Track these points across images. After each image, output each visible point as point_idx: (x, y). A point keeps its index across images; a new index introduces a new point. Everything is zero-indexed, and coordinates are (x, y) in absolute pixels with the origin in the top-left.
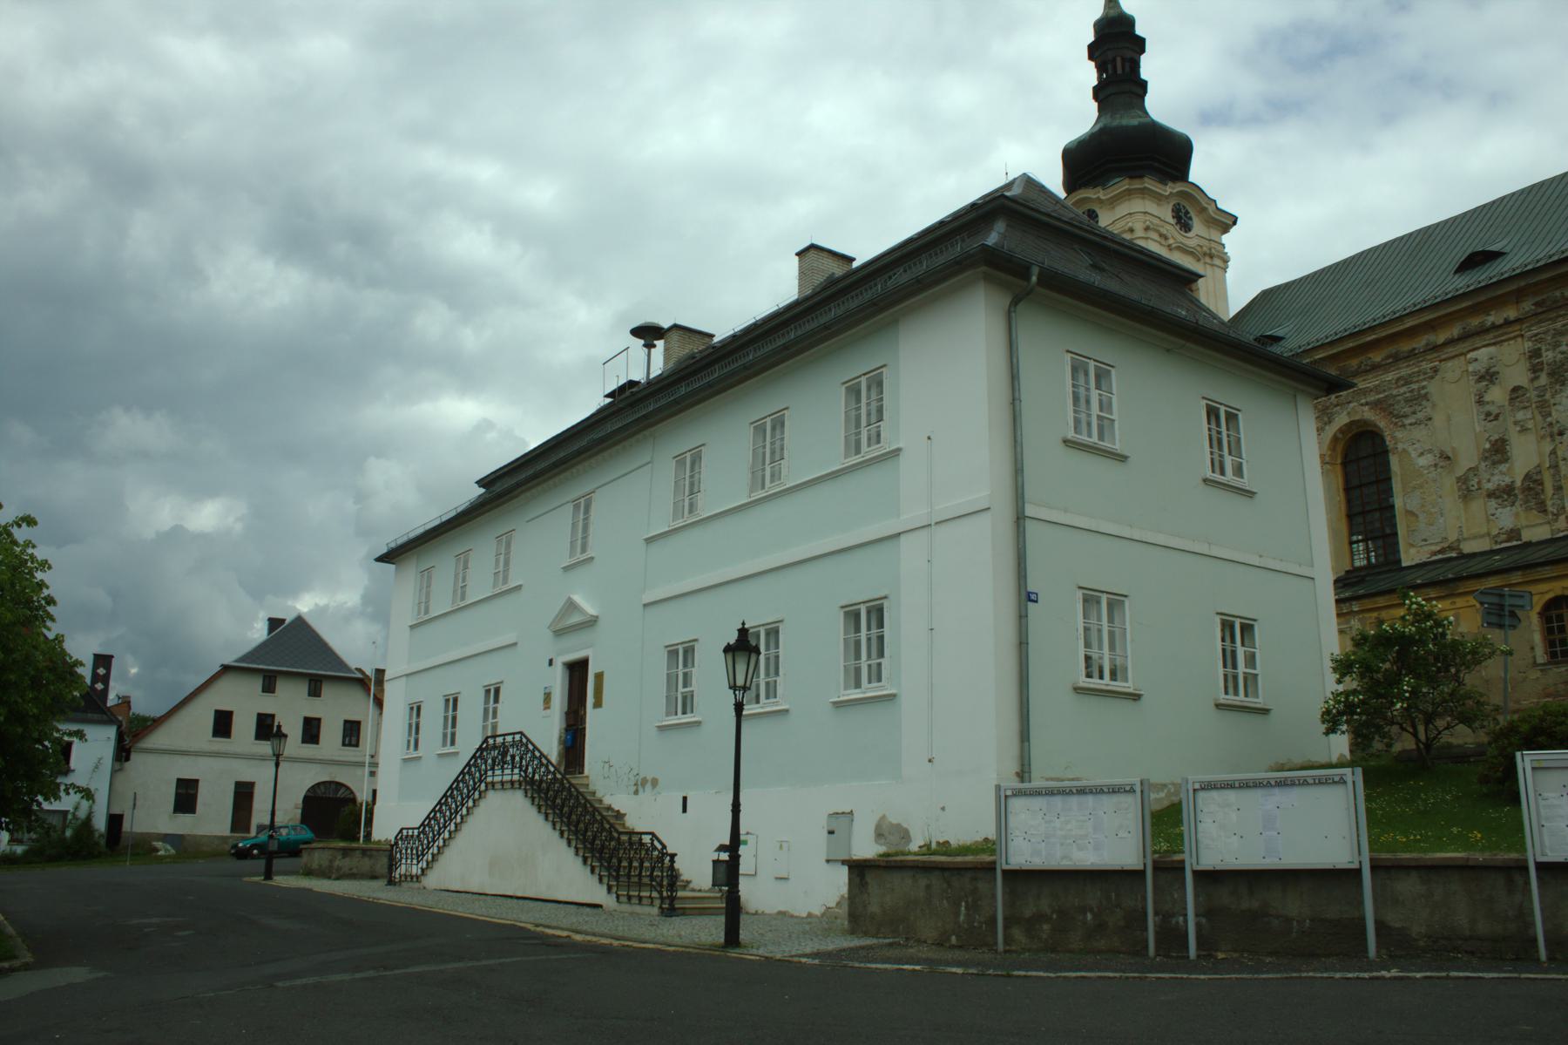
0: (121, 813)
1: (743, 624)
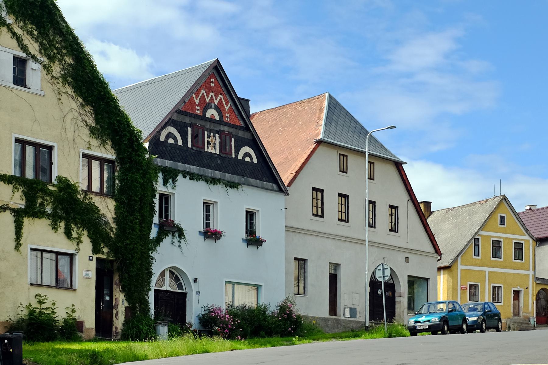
1: (406, 163)
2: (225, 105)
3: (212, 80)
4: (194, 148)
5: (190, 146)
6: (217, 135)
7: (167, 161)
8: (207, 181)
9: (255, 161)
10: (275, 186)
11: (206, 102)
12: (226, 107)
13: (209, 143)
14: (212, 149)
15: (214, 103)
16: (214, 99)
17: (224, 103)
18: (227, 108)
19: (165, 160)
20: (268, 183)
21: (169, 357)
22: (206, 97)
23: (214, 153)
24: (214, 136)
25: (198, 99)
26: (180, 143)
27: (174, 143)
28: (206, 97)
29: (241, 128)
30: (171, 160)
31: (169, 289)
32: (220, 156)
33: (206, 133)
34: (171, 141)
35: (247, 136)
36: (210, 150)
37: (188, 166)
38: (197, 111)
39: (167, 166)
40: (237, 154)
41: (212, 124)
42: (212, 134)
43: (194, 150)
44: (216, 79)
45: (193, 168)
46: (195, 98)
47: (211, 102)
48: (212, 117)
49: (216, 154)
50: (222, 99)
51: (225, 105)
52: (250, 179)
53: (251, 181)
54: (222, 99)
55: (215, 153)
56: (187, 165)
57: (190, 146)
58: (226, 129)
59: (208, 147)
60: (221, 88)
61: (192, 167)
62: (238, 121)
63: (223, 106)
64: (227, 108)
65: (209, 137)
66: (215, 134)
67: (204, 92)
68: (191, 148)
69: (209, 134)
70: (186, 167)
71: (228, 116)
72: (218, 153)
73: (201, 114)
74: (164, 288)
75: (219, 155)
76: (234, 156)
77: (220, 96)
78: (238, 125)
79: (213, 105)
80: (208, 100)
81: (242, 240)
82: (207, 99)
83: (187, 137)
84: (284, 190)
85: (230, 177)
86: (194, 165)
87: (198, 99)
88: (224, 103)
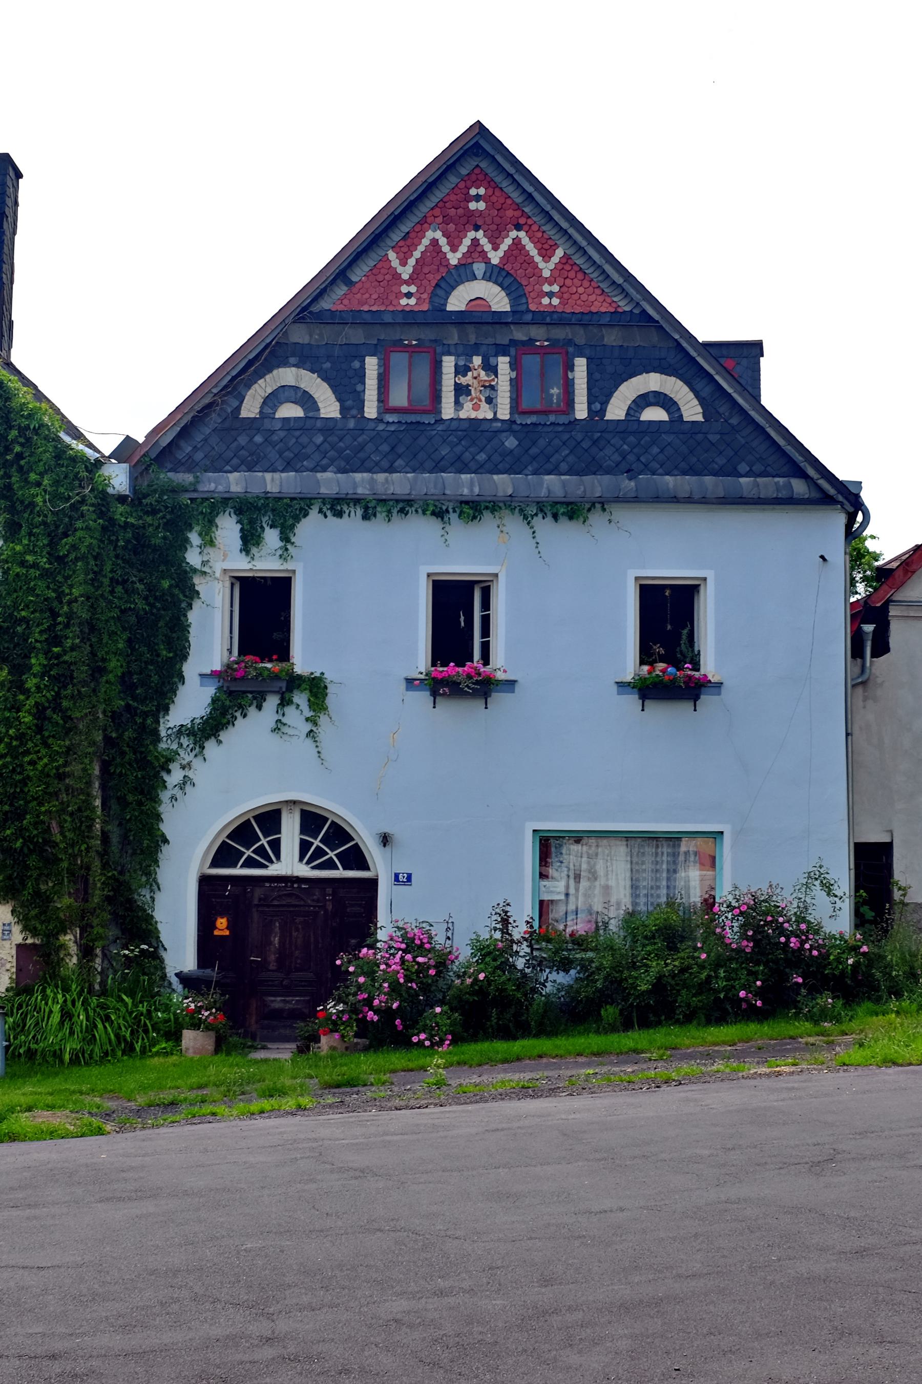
0: (884, 838)
2: (538, 259)
3: (473, 192)
4: (390, 418)
5: (371, 410)
6: (503, 363)
7: (268, 476)
8: (440, 514)
9: (692, 411)
10: (799, 487)
11: (448, 265)
12: (541, 265)
13: (461, 391)
14: (476, 408)
15: (487, 261)
16: (488, 247)
17: (534, 253)
18: (546, 268)
19: (260, 474)
20: (758, 479)
21: (81, 1136)
22: (446, 249)
23: (485, 420)
24: (491, 369)
25: (412, 262)
26: (329, 407)
27: (667, 419)
28: (446, 249)
29: (617, 319)
30: (288, 466)
31: (304, 871)
32: (514, 422)
33: (449, 363)
34: (290, 411)
35: (640, 339)
36: (467, 412)
37: (363, 479)
38: (404, 301)
39: (269, 489)
40: (597, 406)
41: (471, 329)
42: (477, 361)
43: (388, 422)
44: (491, 184)
45: (386, 479)
46: (395, 263)
47: (470, 260)
48: (478, 305)
49: (495, 419)
50: (526, 241)
51: (538, 259)
52: (667, 477)
53: (671, 485)
54: (526, 241)
55: (490, 416)
56: (358, 476)
57: (371, 410)
58: (540, 335)
59: (457, 403)
60: (518, 207)
61: (381, 477)
62: (601, 298)
63: (531, 262)
64: (546, 268)
65: (461, 370)
66: (492, 361)
67: (438, 235)
68: (379, 420)
69: (461, 363)
70: (355, 483)
71: (413, 289)
72: (504, 413)
73: (425, 307)
74: (274, 870)
75: (512, 422)
76: (581, 412)
77: (514, 234)
78: (603, 310)
79: (479, 268)
80: (454, 259)
81: (615, 687)
82: (450, 255)
83: (359, 388)
84: (832, 491)
85: (564, 484)
86: (391, 470)
87: (412, 262)
88: (534, 253)
